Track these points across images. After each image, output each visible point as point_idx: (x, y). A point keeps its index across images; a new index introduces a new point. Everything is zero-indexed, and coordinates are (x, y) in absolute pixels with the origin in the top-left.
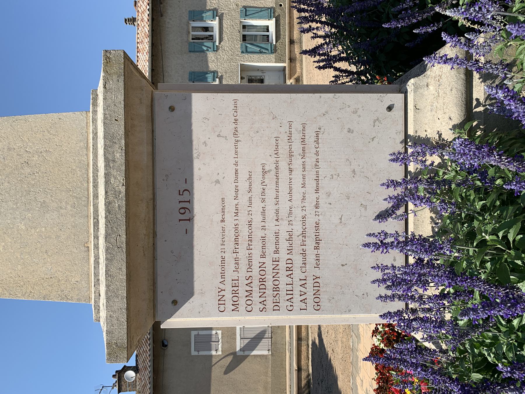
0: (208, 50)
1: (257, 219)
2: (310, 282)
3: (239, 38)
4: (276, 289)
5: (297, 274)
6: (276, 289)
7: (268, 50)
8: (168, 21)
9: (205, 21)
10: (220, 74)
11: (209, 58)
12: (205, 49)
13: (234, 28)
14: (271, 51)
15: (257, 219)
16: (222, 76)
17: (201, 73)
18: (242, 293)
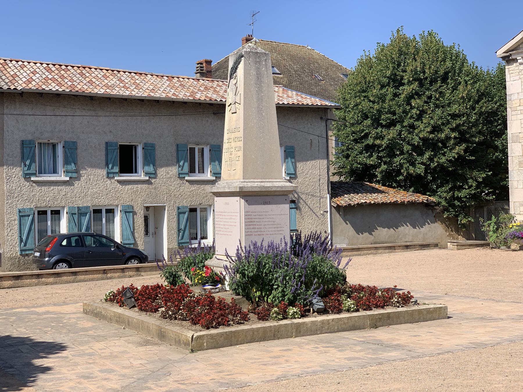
0: (179, 166)
1: (264, 220)
2: (251, 233)
3: (194, 204)
4: (250, 225)
5: (253, 230)
6: (250, 225)
7: (182, 239)
8: (209, 121)
9: (210, 164)
10: (153, 181)
11: (170, 168)
12: (181, 163)
13: (204, 198)
14: (181, 243)
15: (264, 220)
16: (151, 183)
17: (154, 158)
18: (249, 217)
